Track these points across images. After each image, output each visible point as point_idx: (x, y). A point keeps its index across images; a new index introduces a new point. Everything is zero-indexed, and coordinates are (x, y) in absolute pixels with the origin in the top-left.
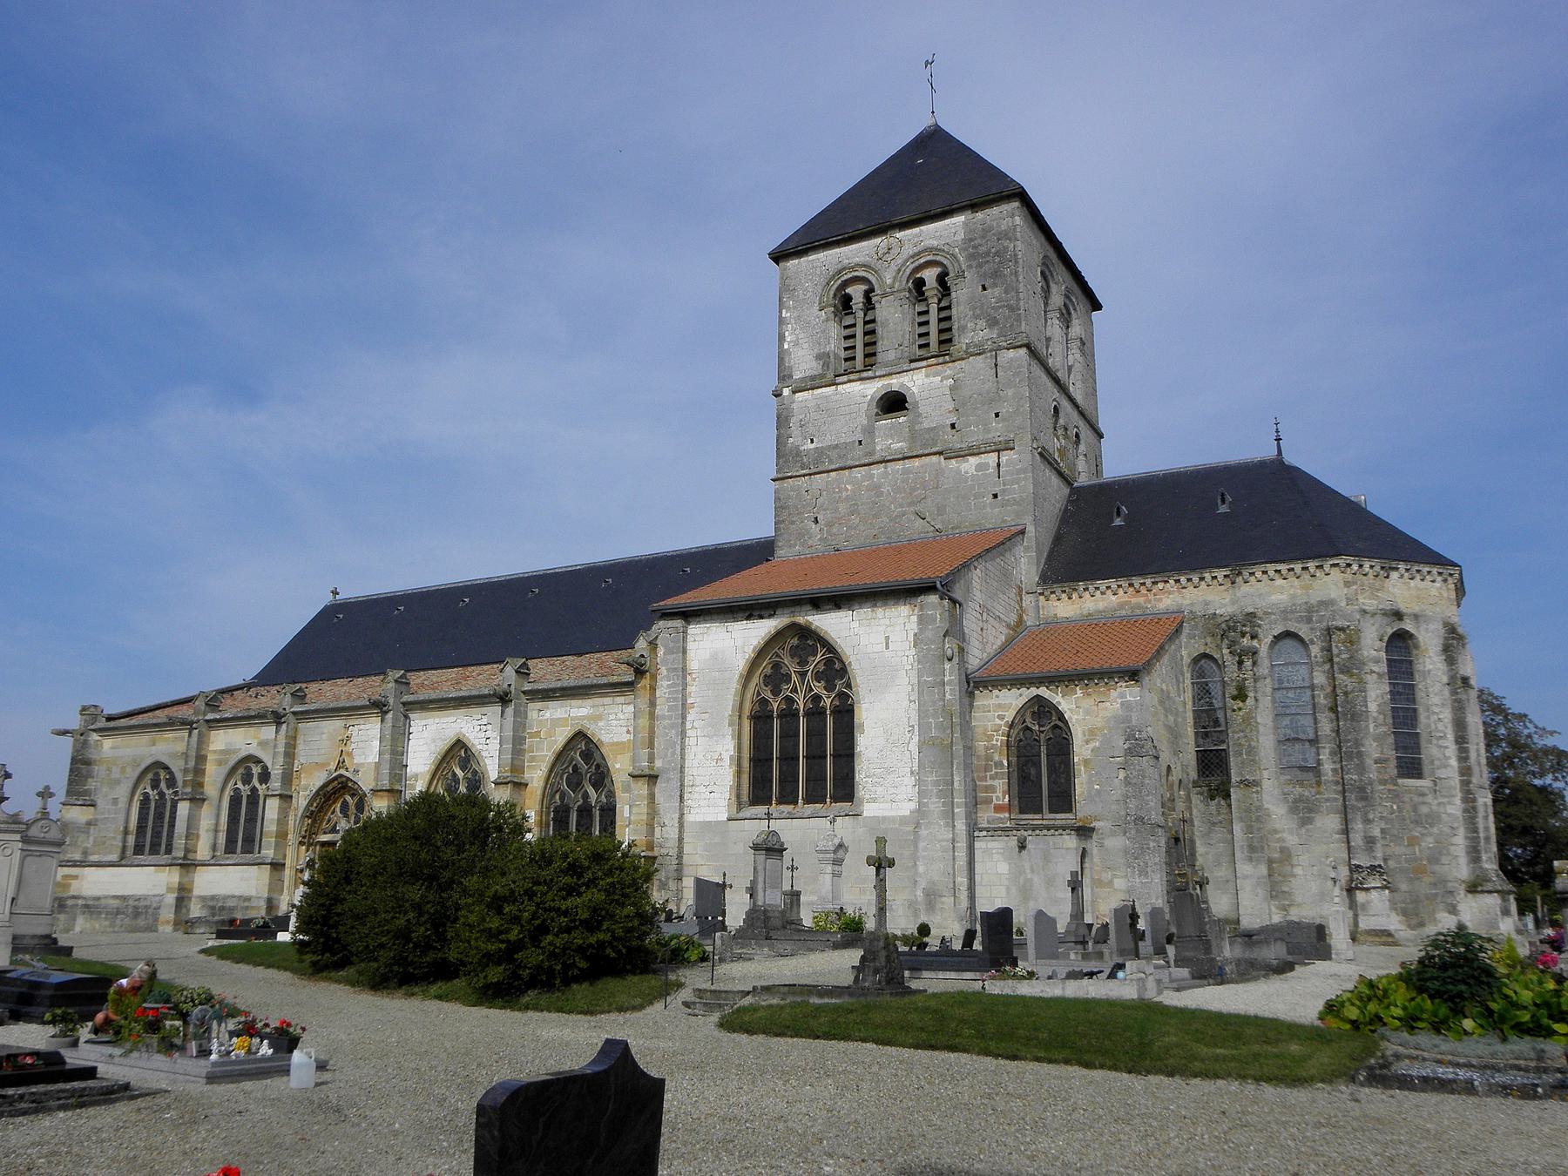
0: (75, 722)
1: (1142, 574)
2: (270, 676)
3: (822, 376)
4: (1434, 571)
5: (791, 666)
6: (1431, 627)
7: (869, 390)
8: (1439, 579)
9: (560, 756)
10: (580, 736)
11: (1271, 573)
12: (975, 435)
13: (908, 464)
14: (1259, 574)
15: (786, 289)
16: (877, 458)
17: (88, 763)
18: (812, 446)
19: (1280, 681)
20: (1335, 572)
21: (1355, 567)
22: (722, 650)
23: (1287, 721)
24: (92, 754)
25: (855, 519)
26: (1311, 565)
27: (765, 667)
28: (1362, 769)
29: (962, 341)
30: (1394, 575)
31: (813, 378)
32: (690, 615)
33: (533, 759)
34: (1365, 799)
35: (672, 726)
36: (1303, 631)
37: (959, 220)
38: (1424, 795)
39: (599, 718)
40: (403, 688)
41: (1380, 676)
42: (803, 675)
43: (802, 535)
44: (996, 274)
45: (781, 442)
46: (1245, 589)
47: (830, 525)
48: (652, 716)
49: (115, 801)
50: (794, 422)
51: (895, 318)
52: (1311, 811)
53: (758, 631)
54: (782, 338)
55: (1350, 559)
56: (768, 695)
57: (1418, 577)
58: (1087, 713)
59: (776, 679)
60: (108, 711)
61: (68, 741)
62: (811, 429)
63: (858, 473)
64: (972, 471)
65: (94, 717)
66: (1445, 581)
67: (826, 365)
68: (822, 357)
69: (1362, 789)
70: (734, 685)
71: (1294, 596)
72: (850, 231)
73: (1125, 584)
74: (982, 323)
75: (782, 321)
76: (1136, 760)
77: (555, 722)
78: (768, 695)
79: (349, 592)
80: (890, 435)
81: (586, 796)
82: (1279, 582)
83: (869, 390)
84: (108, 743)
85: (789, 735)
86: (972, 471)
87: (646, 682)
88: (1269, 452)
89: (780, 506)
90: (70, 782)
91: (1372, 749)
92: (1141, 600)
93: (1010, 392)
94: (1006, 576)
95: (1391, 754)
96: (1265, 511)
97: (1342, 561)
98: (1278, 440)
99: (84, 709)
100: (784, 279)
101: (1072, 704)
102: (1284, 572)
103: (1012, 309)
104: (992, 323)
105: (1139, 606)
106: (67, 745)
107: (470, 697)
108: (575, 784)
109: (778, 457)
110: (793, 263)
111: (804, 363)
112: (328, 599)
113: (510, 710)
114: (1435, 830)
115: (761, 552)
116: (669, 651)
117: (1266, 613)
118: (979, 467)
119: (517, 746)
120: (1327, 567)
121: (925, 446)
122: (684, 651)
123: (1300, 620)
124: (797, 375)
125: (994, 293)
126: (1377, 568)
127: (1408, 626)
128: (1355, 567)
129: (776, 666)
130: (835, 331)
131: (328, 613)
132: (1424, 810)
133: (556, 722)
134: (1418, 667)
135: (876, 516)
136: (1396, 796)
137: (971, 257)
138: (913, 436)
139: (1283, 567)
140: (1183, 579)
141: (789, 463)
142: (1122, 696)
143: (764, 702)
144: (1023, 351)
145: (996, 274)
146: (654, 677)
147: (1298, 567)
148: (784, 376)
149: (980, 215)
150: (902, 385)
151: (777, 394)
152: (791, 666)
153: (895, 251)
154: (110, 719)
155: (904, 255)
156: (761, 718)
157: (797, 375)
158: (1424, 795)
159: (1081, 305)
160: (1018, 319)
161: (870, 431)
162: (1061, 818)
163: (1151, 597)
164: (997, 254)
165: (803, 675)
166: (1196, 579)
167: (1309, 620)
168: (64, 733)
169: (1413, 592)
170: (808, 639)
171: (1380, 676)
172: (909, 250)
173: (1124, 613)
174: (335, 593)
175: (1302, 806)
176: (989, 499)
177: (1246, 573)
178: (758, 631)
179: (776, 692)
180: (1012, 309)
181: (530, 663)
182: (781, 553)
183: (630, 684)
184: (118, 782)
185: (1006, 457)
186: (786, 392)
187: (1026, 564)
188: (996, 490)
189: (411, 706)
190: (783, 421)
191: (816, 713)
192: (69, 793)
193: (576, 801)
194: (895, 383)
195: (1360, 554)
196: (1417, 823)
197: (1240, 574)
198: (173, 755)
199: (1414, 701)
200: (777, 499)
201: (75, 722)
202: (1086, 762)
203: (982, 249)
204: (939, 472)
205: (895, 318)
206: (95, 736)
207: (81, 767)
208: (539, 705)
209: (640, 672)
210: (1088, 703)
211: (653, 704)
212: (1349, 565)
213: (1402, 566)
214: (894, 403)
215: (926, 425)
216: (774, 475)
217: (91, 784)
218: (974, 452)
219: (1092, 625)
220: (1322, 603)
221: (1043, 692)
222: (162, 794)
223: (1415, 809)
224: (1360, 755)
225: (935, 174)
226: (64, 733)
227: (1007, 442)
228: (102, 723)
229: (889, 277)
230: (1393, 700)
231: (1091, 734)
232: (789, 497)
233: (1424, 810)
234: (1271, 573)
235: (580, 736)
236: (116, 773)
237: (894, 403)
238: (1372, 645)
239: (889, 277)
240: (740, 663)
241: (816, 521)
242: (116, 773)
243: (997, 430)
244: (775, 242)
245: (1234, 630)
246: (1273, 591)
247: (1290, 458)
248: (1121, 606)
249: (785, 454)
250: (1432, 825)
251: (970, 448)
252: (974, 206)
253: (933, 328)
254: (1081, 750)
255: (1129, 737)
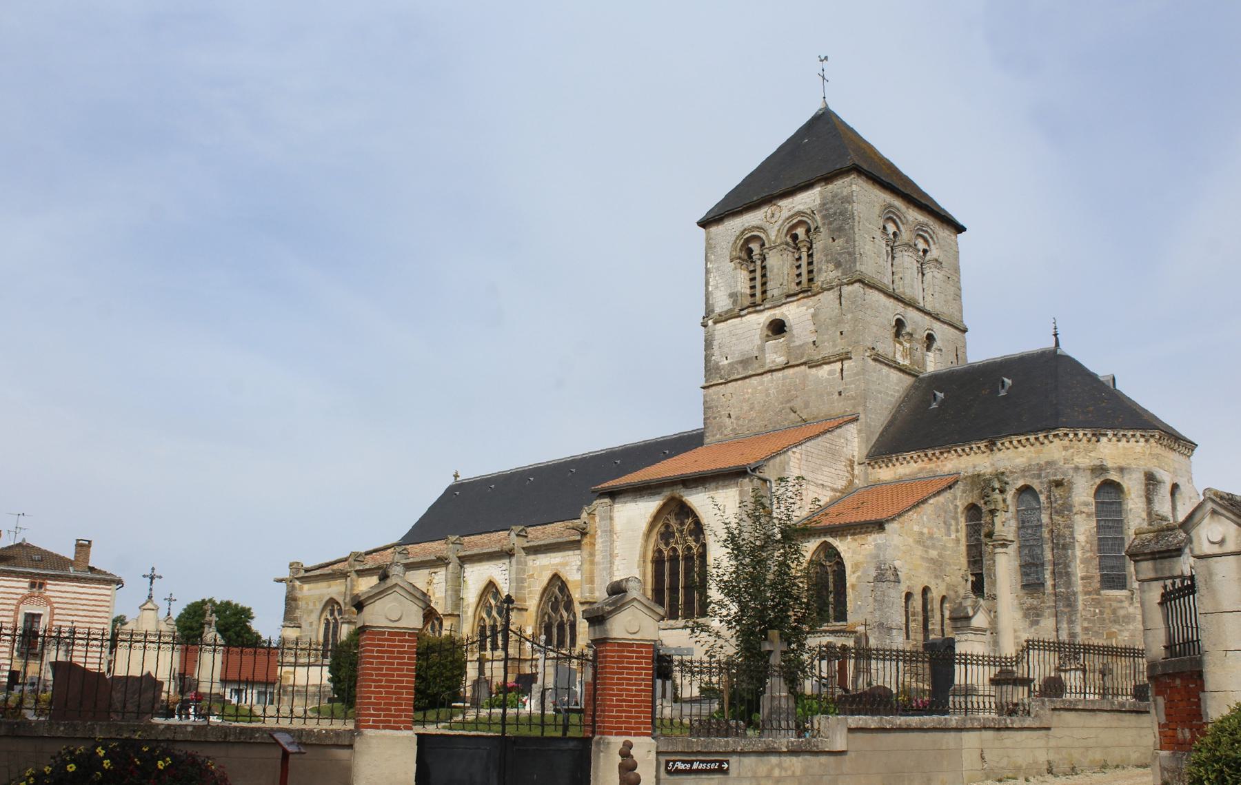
0: (286, 573)
1: (932, 447)
2: (425, 529)
3: (730, 310)
4: (1138, 434)
5: (675, 525)
6: (1134, 476)
7: (764, 318)
8: (1142, 440)
9: (545, 590)
10: (556, 577)
11: (1015, 443)
12: (827, 350)
13: (787, 372)
14: (1007, 444)
15: (709, 247)
16: (767, 368)
17: (295, 599)
18: (726, 362)
19: (1023, 522)
20: (1056, 440)
21: (1071, 436)
22: (632, 519)
23: (1026, 551)
24: (298, 594)
25: (753, 414)
26: (1041, 436)
27: (659, 527)
28: (1069, 584)
29: (820, 280)
30: (1104, 439)
31: (727, 312)
32: (613, 495)
33: (530, 592)
34: (1069, 605)
35: (604, 569)
36: (1036, 484)
37: (816, 191)
38: (1121, 601)
39: (566, 564)
40: (459, 547)
41: (1089, 515)
42: (681, 532)
43: (721, 427)
44: (840, 229)
45: (707, 359)
46: (1000, 455)
47: (738, 418)
48: (592, 563)
49: (311, 624)
50: (716, 347)
51: (780, 265)
52: (1038, 615)
53: (647, 508)
54: (707, 283)
55: (1066, 430)
56: (663, 547)
57: (1124, 440)
58: (854, 552)
59: (666, 536)
60: (307, 565)
61: (284, 585)
62: (726, 350)
63: (755, 380)
64: (826, 376)
65: (298, 570)
66: (1147, 441)
67: (735, 302)
68: (733, 296)
69: (1068, 599)
70: (640, 541)
71: (1030, 459)
72: (788, 185)
73: (922, 455)
74: (831, 266)
75: (707, 271)
76: (880, 584)
77: (476, 577)
78: (663, 547)
79: (467, 474)
80: (775, 353)
81: (562, 617)
82: (1021, 449)
83: (764, 318)
84: (306, 587)
85: (674, 574)
86: (826, 376)
87: (586, 540)
88: (1051, 344)
89: (707, 408)
90: (286, 613)
91: (1078, 570)
92: (932, 465)
93: (849, 316)
94: (833, 454)
95: (1096, 573)
96: (1047, 392)
97: (1061, 432)
98: (1056, 335)
99: (291, 565)
100: (708, 239)
101: (844, 546)
102: (1023, 442)
103: (849, 253)
104: (838, 265)
105: (931, 470)
106: (283, 588)
107: (422, 562)
108: (555, 608)
109: (706, 371)
110: (714, 229)
111: (722, 303)
112: (450, 481)
113: (514, 560)
114: (1131, 627)
115: (690, 441)
116: (602, 519)
117: (1011, 472)
118: (831, 373)
119: (519, 582)
120: (1051, 437)
121: (796, 358)
122: (611, 518)
123: (1033, 476)
124: (718, 310)
125: (840, 242)
126: (1089, 435)
127: (1113, 476)
128: (1071, 436)
129: (667, 526)
130: (743, 276)
131: (450, 491)
132: (1122, 612)
133: (543, 568)
134: (1125, 507)
135: (766, 411)
136: (1098, 603)
137: (824, 217)
138: (789, 351)
139: (1023, 438)
140: (959, 450)
141: (714, 375)
142: (875, 540)
143: (660, 551)
144: (857, 285)
145: (840, 229)
146: (593, 536)
147: (1032, 438)
148: (709, 312)
149: (830, 186)
150: (783, 314)
151: (705, 325)
152: (675, 525)
153: (777, 215)
154: (306, 571)
155: (783, 218)
156: (658, 562)
157: (718, 310)
158: (1121, 601)
159: (943, 233)
160: (855, 262)
161: (762, 349)
162: (839, 625)
163: (939, 463)
164: (841, 214)
165: (681, 532)
166: (967, 449)
167: (1039, 476)
168: (280, 581)
169: (1118, 452)
170: (685, 511)
171: (1089, 515)
172: (785, 214)
173: (922, 475)
174: (456, 476)
175: (1031, 612)
176: (836, 396)
177: (999, 445)
178: (647, 508)
179: (667, 544)
180: (849, 253)
181: (529, 530)
182: (707, 440)
183: (579, 541)
184: (312, 611)
185: (847, 364)
186: (710, 323)
187: (853, 442)
188: (840, 389)
189: (464, 560)
190: (708, 344)
191: (688, 559)
192: (285, 619)
193: (488, 622)
194: (777, 313)
195: (1075, 426)
196: (1116, 621)
197: (994, 444)
198: (339, 594)
199: (1122, 533)
200: (705, 402)
201: (286, 573)
202: (853, 586)
203: (831, 211)
204: (805, 377)
205: (780, 265)
206: (297, 583)
207: (291, 601)
208: (532, 557)
209: (584, 533)
210: (855, 544)
211: (592, 554)
212: (1066, 435)
213: (1110, 433)
214: (778, 328)
215: (797, 343)
216: (704, 384)
217: (298, 613)
218: (826, 361)
219: (900, 483)
220: (1048, 463)
221: (830, 540)
222: (335, 619)
223: (1114, 611)
224: (1068, 574)
225: (823, 151)
226: (280, 581)
227: (847, 353)
228: (302, 574)
229: (774, 234)
230: (1098, 532)
231: (856, 566)
232: (712, 400)
233: (1122, 612)
234: (1015, 443)
235: (556, 577)
236: (311, 606)
237: (778, 328)
238: (1083, 493)
239: (774, 234)
240: (643, 525)
241: (729, 416)
242: (311, 606)
243: (841, 346)
244: (701, 215)
245: (985, 486)
246: (1015, 457)
247: (1066, 349)
248: (921, 470)
249: (710, 368)
250: (1128, 623)
251: (823, 358)
252: (828, 179)
253: (804, 270)
254: (850, 579)
255: (879, 568)
